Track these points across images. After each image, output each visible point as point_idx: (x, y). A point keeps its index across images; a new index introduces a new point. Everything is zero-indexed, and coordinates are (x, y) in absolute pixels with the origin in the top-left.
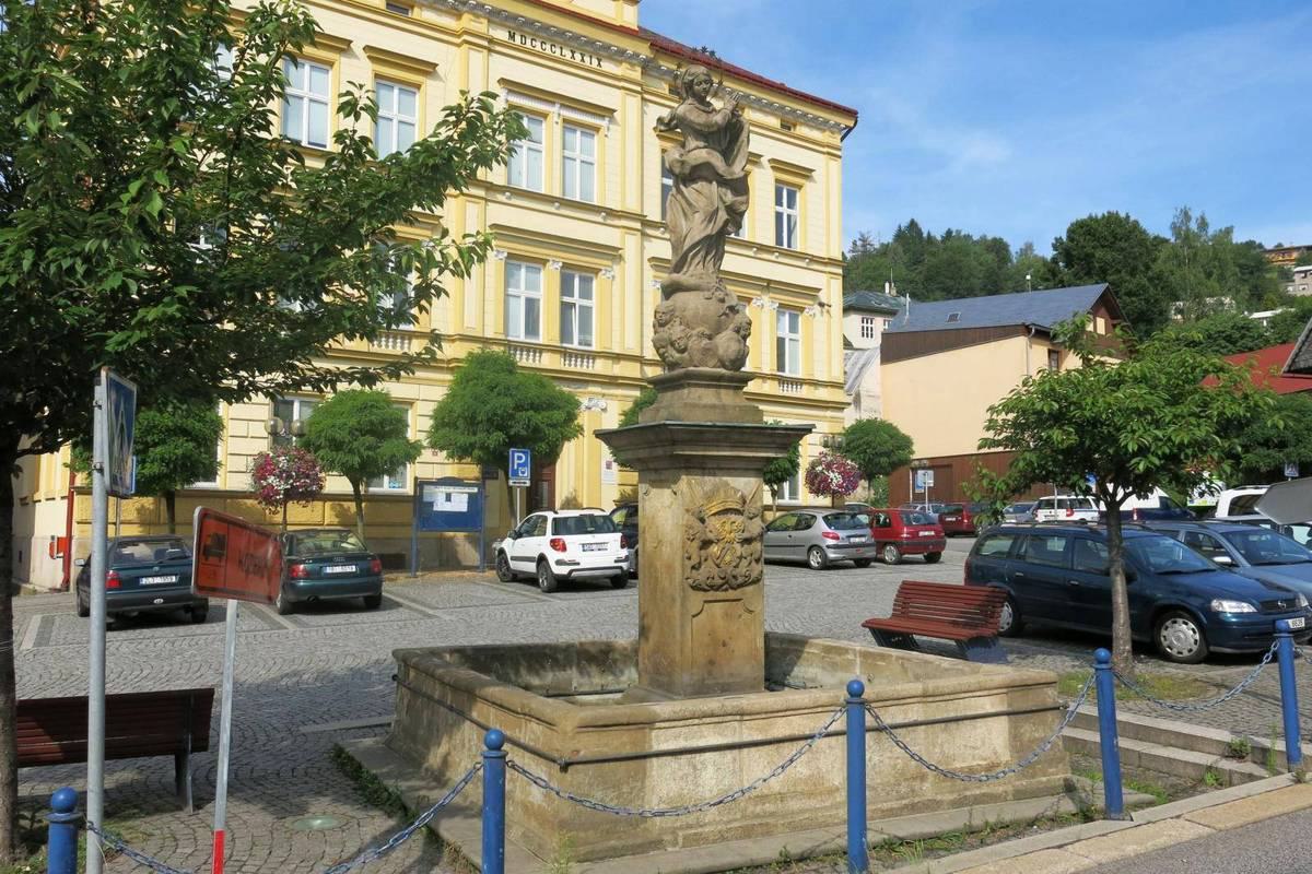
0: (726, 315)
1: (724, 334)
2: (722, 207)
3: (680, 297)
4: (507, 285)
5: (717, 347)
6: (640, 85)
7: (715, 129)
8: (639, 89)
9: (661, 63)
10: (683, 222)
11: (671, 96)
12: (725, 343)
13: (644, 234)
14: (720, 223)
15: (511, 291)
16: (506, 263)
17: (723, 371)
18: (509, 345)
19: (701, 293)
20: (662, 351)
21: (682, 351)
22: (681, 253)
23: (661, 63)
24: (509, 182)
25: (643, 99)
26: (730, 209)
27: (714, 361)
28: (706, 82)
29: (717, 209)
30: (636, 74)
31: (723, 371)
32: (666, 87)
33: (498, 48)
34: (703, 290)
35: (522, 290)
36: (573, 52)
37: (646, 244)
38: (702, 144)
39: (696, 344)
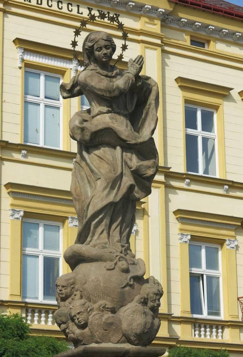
0: (131, 286)
1: (129, 306)
2: (127, 172)
3: (83, 268)
4: (24, 244)
5: (120, 321)
6: (161, 38)
7: (117, 93)
8: (159, 42)
9: (181, 15)
10: (89, 189)
11: (193, 47)
12: (132, 317)
13: (168, 187)
14: (124, 189)
15: (29, 250)
16: (22, 222)
17: (127, 346)
18: (27, 307)
19: (104, 264)
20: (63, 326)
21: (83, 326)
22: (85, 221)
23: (181, 15)
24: (26, 140)
25: (163, 51)
26: (137, 174)
27: (119, 336)
28: (106, 47)
29: (122, 175)
30: (156, 27)
31: (127, 346)
32: (188, 38)
33: (14, 10)
34: (105, 261)
35: (40, 250)
36: (90, 10)
37: (171, 196)
38: (105, 109)
39: (96, 319)
